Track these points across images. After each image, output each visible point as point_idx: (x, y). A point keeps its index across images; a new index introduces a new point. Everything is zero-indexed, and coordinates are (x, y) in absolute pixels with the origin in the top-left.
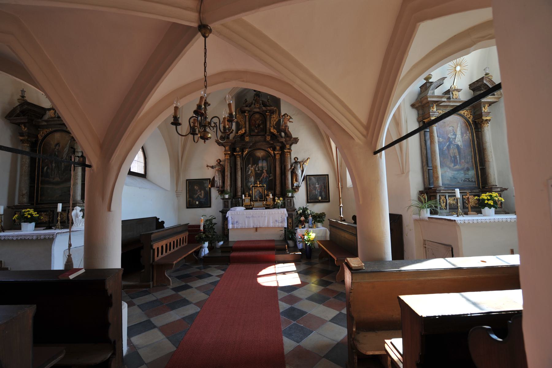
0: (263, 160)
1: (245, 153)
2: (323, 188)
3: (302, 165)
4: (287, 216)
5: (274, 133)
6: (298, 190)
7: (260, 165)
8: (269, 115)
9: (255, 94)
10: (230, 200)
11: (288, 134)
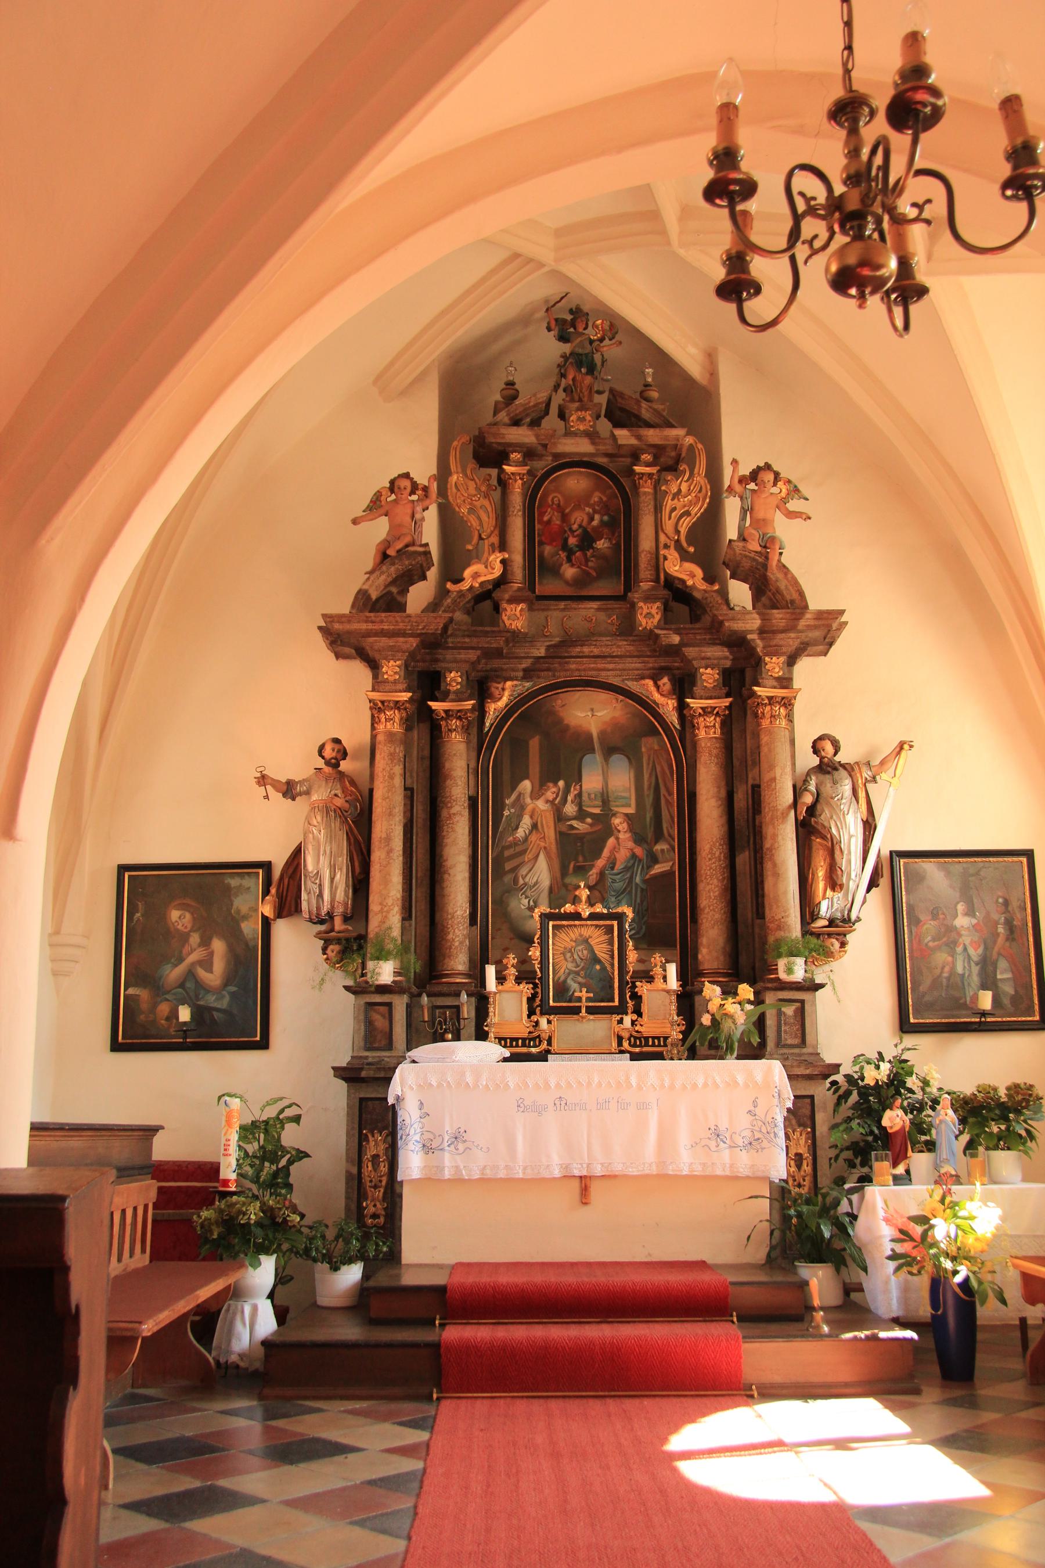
0: (609, 751)
1: (495, 708)
2: (1000, 940)
4: (790, 1105)
5: (683, 582)
6: (843, 944)
7: (592, 781)
8: (650, 476)
9: (564, 356)
10: (405, 998)
11: (778, 591)
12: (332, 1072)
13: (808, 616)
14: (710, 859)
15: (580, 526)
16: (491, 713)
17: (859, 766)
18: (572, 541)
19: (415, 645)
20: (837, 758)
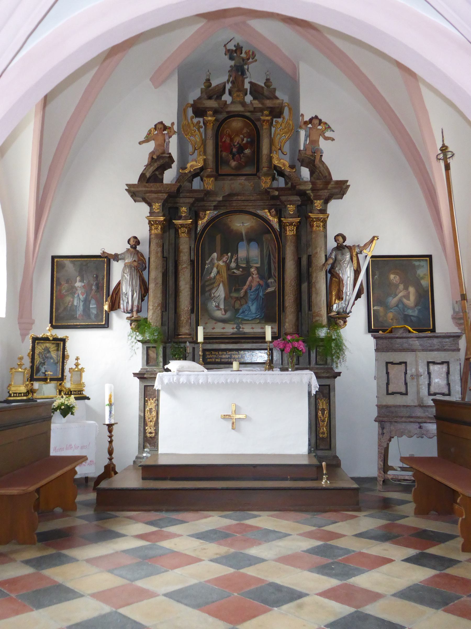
0: (250, 240)
3: (357, 255)
5: (280, 168)
6: (345, 322)
7: (242, 253)
8: (268, 121)
9: (231, 67)
12: (133, 375)
13: (332, 183)
14: (290, 286)
15: (238, 143)
16: (200, 225)
17: (354, 247)
18: (234, 150)
19: (166, 197)
20: (344, 244)
